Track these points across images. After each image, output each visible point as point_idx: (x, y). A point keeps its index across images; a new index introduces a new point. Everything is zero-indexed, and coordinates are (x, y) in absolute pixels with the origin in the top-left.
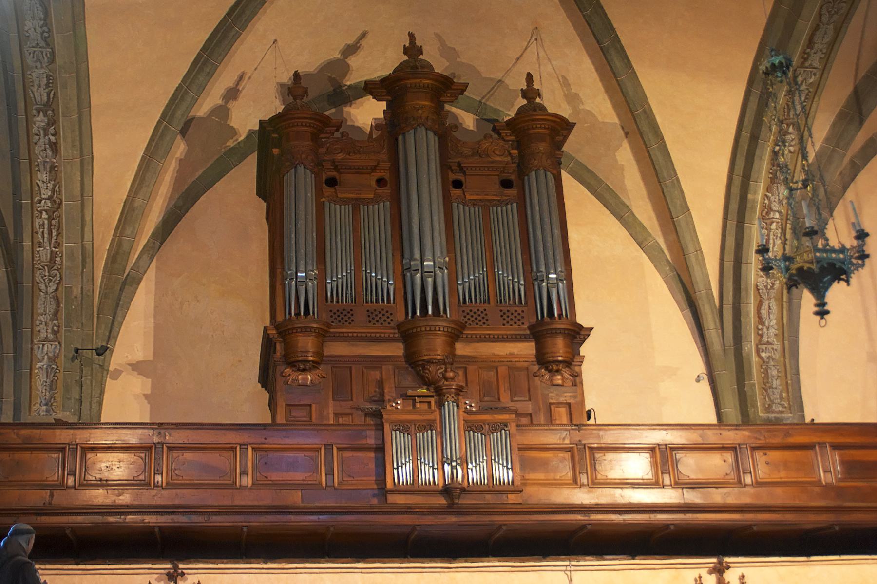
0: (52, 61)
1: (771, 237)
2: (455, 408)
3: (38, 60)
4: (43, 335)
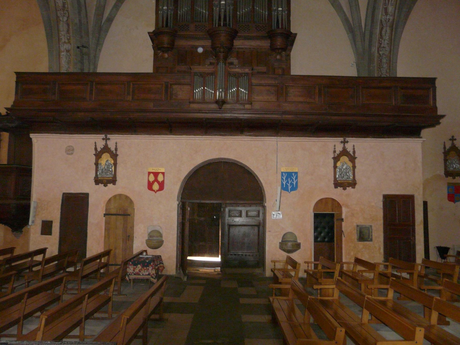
2: (224, 66)
4: (63, 40)
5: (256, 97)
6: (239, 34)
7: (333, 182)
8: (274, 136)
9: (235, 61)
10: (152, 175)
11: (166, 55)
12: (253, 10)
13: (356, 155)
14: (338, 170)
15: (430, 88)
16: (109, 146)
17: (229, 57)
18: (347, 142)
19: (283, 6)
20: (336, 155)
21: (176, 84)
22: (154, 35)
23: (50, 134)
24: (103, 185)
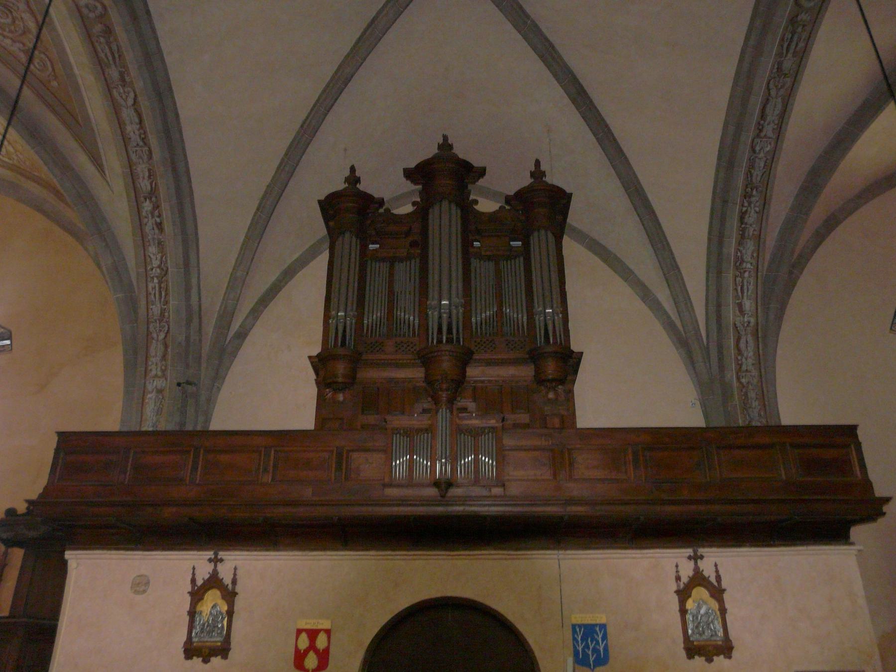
0: (150, 157)
1: (745, 283)
2: (448, 415)
3: (140, 157)
4: (154, 372)
5: (513, 473)
6: (476, 356)
7: (682, 645)
8: (554, 549)
9: (471, 406)
10: (304, 636)
11: (341, 397)
12: (500, 313)
13: (724, 584)
14: (689, 617)
15: (849, 445)
16: (221, 576)
17: (459, 399)
18: (702, 557)
19: (555, 306)
20: (682, 586)
21: (357, 450)
22: (320, 361)
23: (105, 552)
24: (201, 659)
